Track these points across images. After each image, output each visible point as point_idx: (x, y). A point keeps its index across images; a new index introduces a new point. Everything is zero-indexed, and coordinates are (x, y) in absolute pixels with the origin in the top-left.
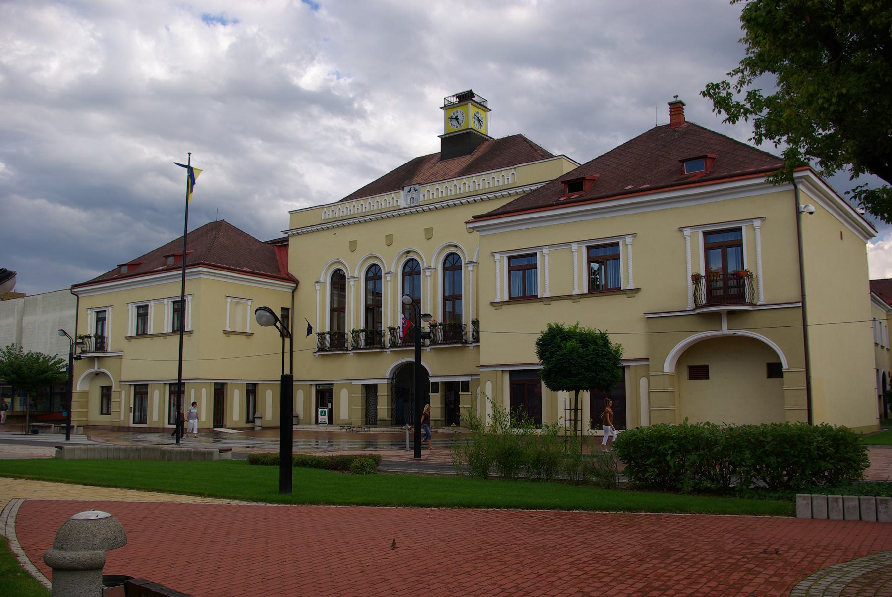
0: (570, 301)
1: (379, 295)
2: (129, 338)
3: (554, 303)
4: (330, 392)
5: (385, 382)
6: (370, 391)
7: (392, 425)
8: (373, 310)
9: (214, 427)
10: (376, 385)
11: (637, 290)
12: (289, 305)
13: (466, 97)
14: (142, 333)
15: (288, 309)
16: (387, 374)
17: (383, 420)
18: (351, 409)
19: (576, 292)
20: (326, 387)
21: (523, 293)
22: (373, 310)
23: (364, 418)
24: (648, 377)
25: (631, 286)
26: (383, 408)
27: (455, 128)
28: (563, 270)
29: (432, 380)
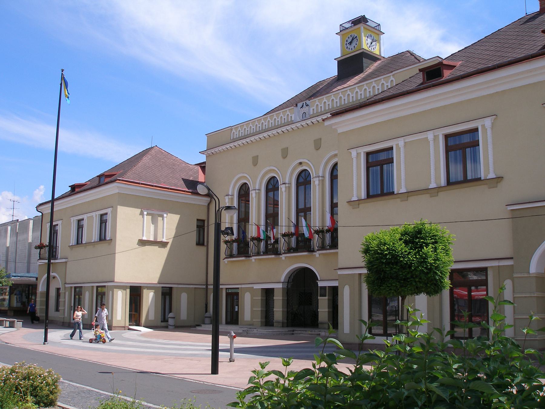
0: (428, 195)
1: (276, 204)
2: (71, 247)
3: (412, 199)
4: (237, 294)
5: (280, 286)
6: (268, 293)
7: (287, 326)
8: (272, 218)
9: (130, 325)
10: (171, 287)
11: (499, 179)
12: (203, 217)
13: (361, 20)
14: (79, 242)
15: (204, 221)
16: (282, 279)
17: (278, 322)
18: (252, 312)
19: (433, 185)
20: (233, 291)
21: (379, 186)
22: (272, 218)
23: (264, 320)
24: (513, 279)
25: (491, 175)
26: (279, 311)
27: (352, 51)
28: (420, 163)
29: (321, 284)
